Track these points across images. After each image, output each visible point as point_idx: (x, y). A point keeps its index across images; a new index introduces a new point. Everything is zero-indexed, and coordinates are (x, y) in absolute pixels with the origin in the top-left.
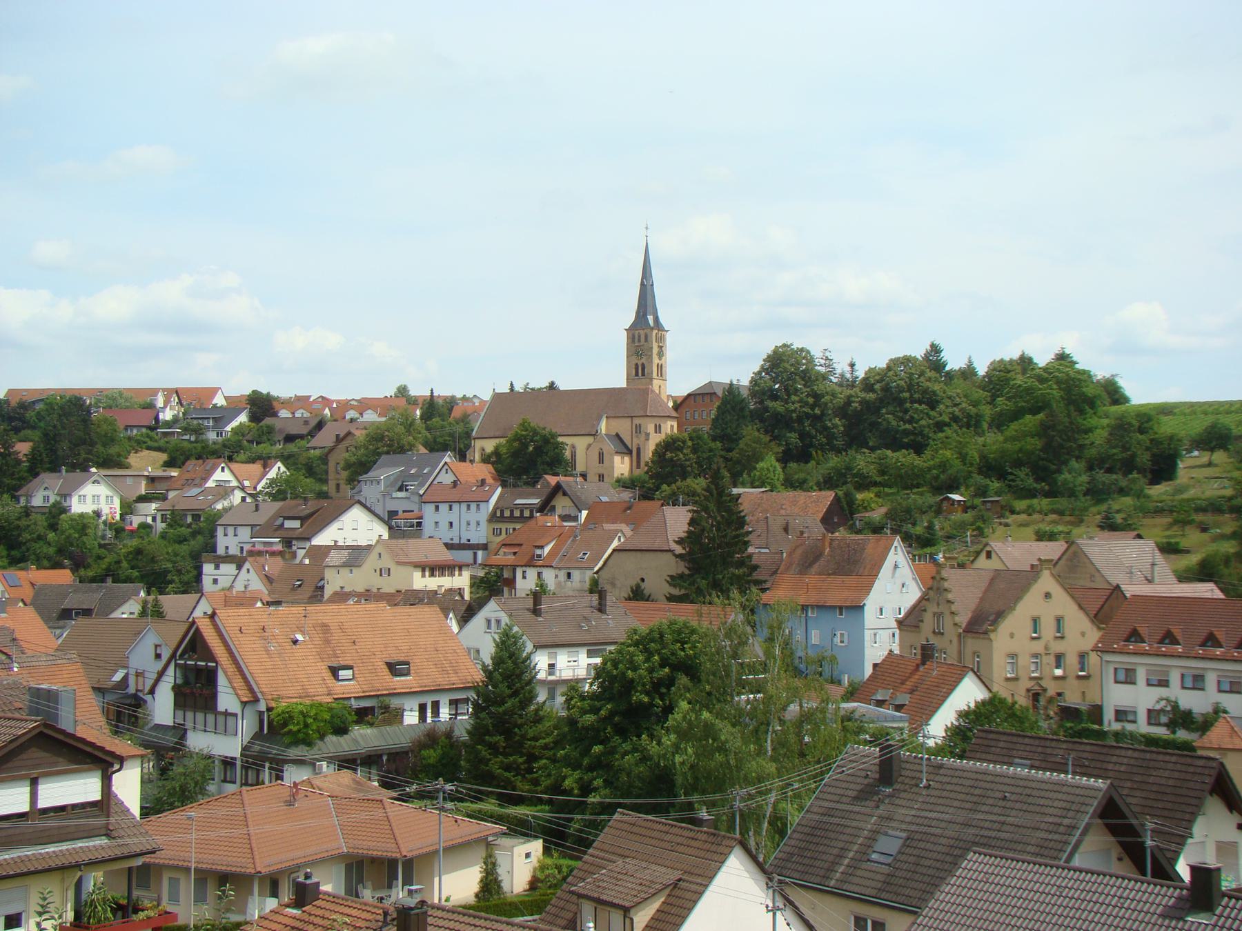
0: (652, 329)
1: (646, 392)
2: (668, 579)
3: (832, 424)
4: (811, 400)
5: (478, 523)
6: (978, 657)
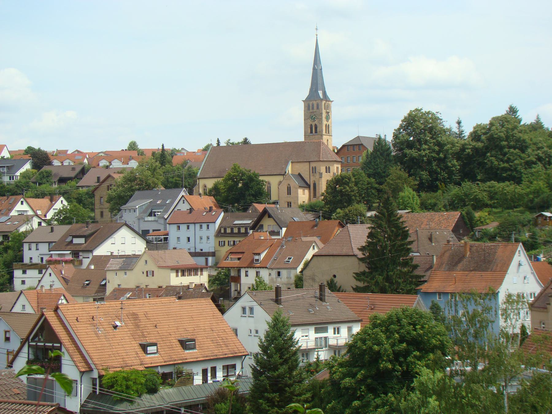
0: (322, 100)
1: (319, 144)
2: (355, 275)
3: (452, 164)
4: (437, 148)
5: (208, 238)
6: (544, 324)
